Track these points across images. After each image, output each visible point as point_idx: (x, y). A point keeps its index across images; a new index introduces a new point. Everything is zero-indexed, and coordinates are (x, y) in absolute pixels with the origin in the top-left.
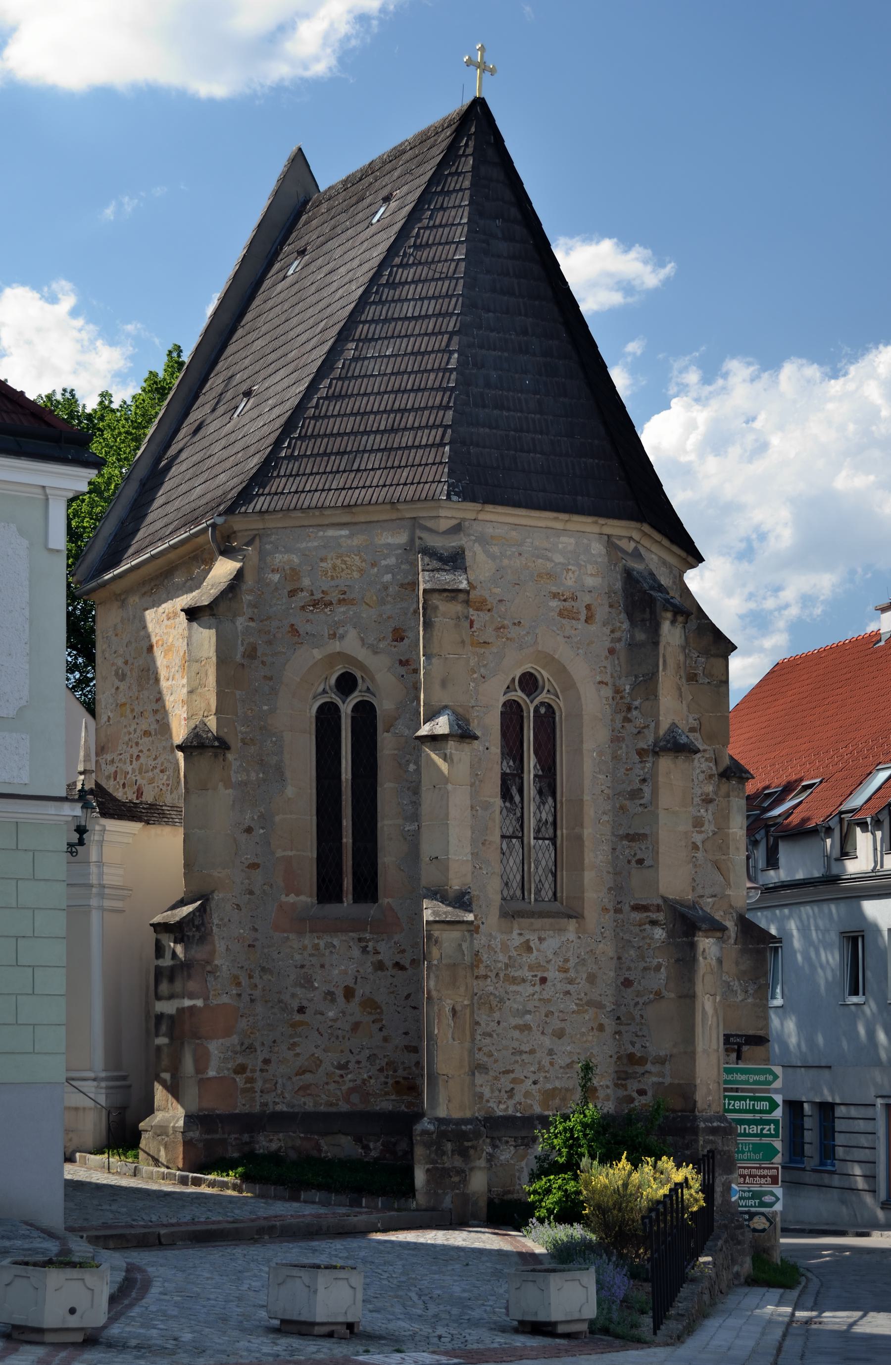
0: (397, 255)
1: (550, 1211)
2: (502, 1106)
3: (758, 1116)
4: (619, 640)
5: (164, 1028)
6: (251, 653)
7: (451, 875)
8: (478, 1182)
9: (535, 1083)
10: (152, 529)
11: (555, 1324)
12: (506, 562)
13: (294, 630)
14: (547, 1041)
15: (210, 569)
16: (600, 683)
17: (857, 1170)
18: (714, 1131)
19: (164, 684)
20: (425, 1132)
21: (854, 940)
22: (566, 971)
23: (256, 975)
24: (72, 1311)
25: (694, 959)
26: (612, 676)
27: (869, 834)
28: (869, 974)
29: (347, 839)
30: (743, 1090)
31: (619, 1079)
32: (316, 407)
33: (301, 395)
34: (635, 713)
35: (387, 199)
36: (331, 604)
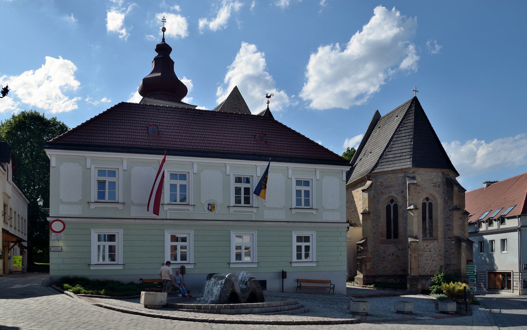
0: (400, 126)
1: (434, 292)
2: (423, 273)
3: (471, 274)
4: (445, 190)
5: (359, 261)
6: (374, 197)
7: (414, 233)
8: (420, 287)
9: (429, 269)
10: (353, 177)
11: (448, 312)
12: (423, 178)
13: (382, 192)
14: (431, 262)
15: (366, 183)
16: (441, 198)
17: (482, 284)
18: (465, 277)
19: (356, 203)
20: (409, 278)
21: (481, 243)
22: (435, 249)
23: (375, 252)
24: (364, 310)
25: (461, 247)
26: (444, 197)
27: (485, 223)
28: (485, 249)
29: (392, 228)
30: (468, 270)
31: (445, 268)
32: (386, 153)
33: (382, 152)
34: (448, 203)
35: (397, 116)
36: (389, 187)
